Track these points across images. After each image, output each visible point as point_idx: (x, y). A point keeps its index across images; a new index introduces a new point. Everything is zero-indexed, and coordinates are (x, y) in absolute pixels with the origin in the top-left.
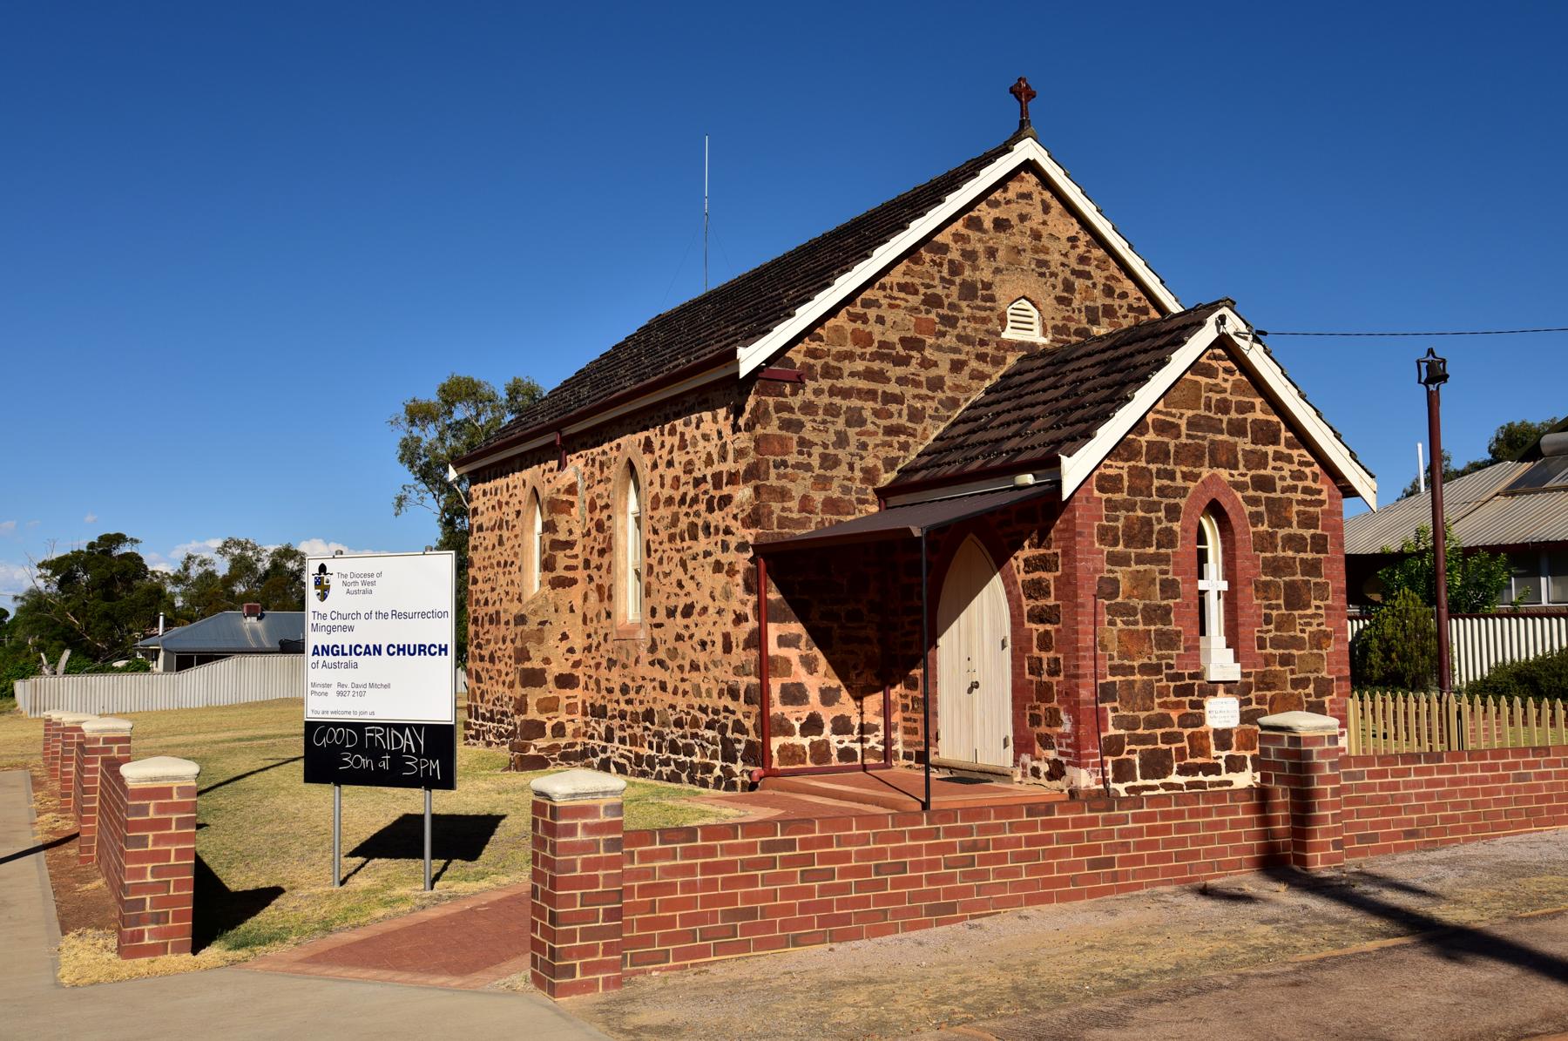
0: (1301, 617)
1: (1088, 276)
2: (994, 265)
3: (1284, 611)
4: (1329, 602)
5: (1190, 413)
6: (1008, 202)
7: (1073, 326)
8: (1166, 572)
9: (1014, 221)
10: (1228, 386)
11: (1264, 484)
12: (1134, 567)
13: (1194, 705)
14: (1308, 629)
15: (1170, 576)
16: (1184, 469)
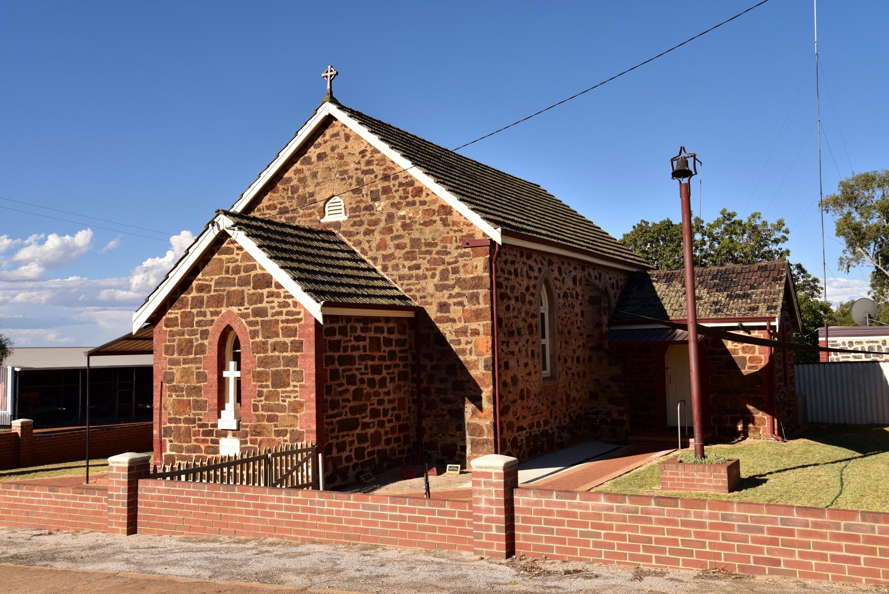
1: (371, 172)
2: (316, 181)
3: (271, 389)
4: (303, 383)
5: (217, 277)
6: (325, 142)
7: (362, 205)
8: (200, 368)
9: (328, 151)
10: (239, 257)
11: (259, 313)
12: (183, 366)
13: (213, 441)
14: (287, 400)
15: (201, 370)
16: (211, 309)
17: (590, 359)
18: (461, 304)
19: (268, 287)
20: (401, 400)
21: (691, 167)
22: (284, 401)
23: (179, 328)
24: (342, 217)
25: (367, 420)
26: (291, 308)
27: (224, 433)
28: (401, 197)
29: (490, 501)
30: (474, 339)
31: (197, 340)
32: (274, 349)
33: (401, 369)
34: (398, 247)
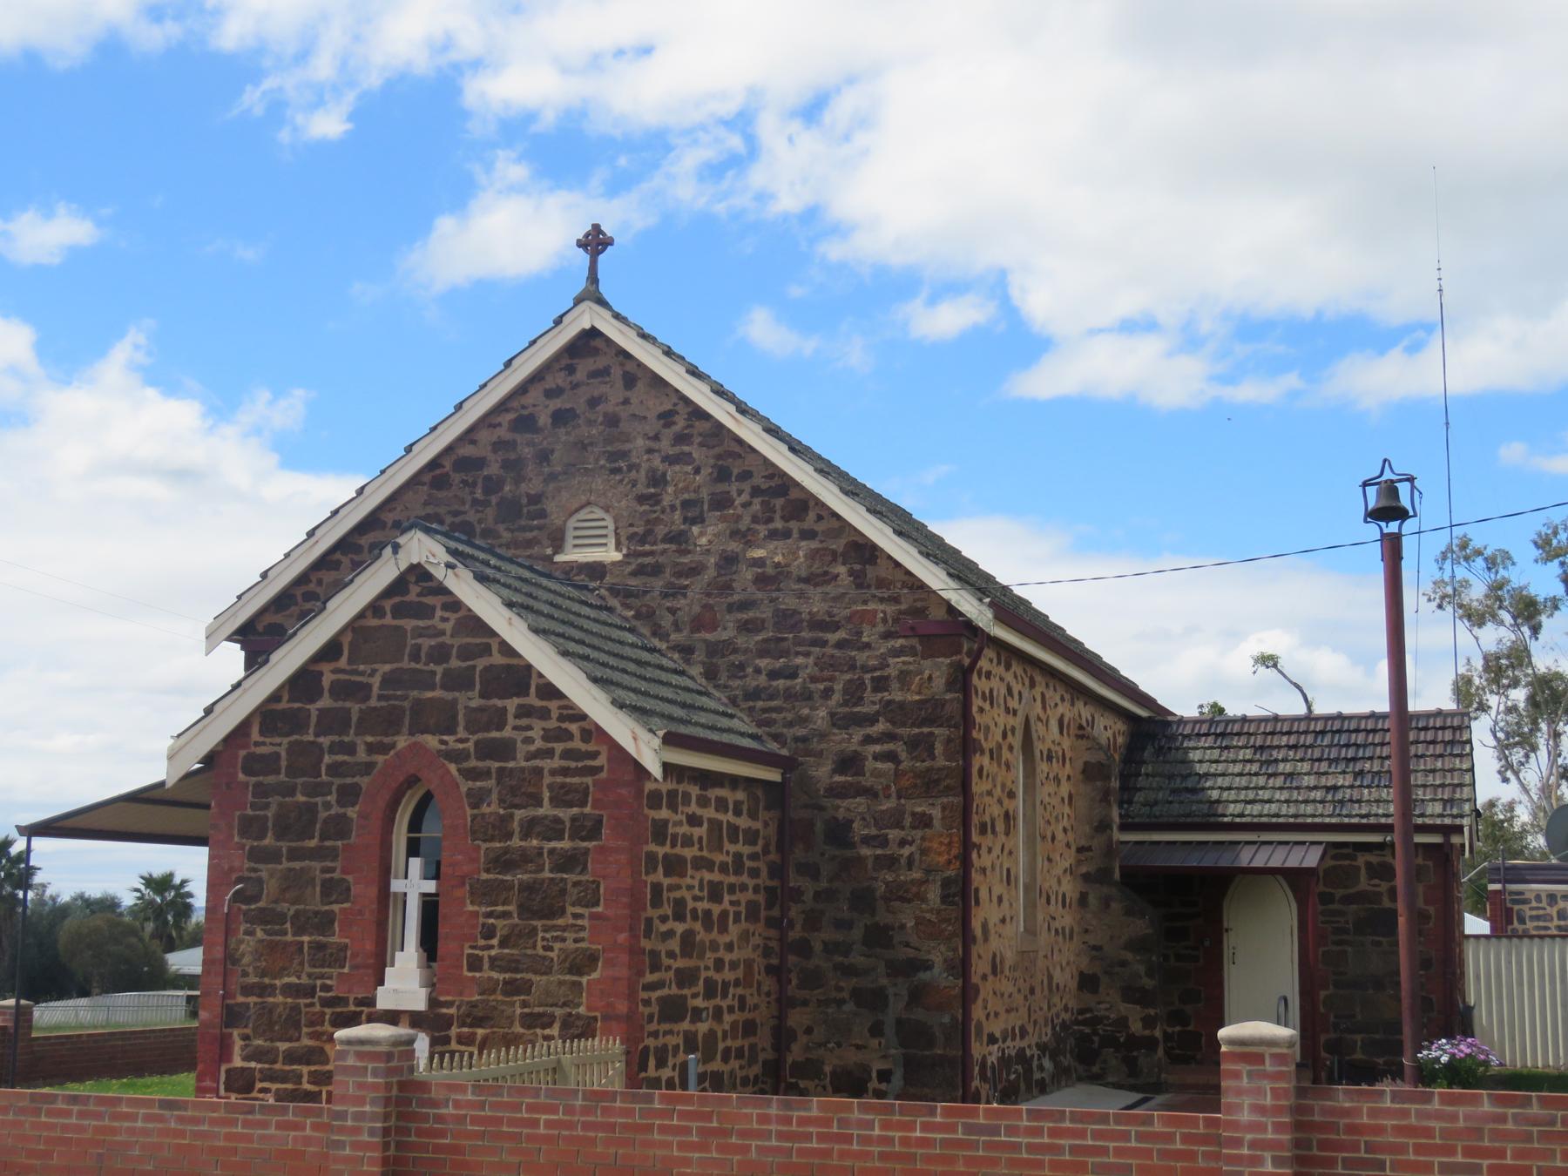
3: (516, 920)
4: (600, 909)
5: (387, 667)
6: (575, 386)
7: (661, 531)
10: (448, 626)
11: (491, 750)
12: (286, 864)
14: (557, 946)
15: (336, 875)
16: (369, 739)
17: (1083, 900)
18: (891, 757)
19: (518, 695)
20: (749, 964)
21: (1405, 501)
22: (548, 948)
23: (282, 777)
24: (610, 554)
25: (699, 1002)
26: (577, 744)
28: (755, 519)
29: (1261, 1110)
30: (919, 834)
31: (328, 806)
32: (526, 836)
33: (750, 895)
34: (746, 627)
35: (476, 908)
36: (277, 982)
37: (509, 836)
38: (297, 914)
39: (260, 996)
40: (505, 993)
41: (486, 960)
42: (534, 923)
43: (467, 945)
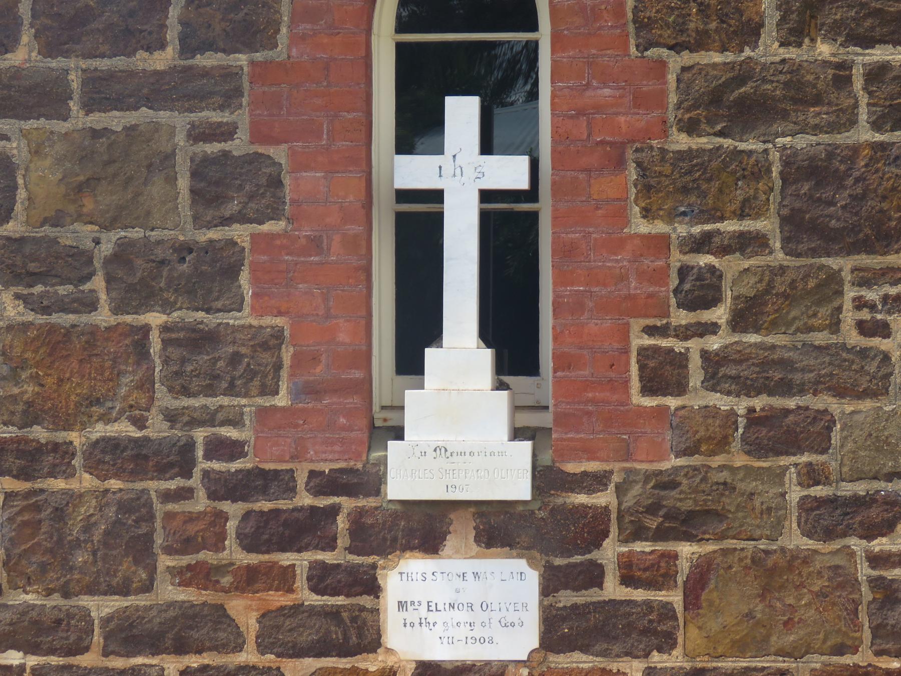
0: (865, 279)
3: (779, 257)
12: (79, 119)
15: (239, 145)
27: (426, 527)
35: (660, 227)
36: (75, 437)
37: (751, 32)
38: (122, 256)
39: (23, 474)
40: (755, 448)
41: (695, 363)
42: (833, 263)
43: (637, 325)
